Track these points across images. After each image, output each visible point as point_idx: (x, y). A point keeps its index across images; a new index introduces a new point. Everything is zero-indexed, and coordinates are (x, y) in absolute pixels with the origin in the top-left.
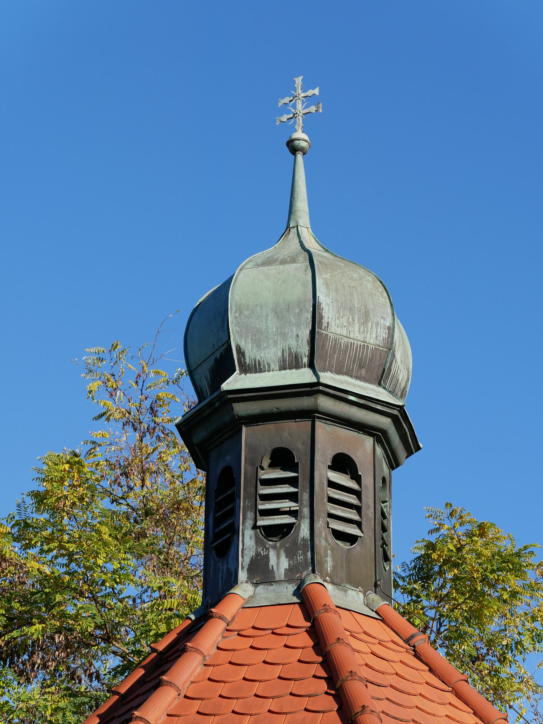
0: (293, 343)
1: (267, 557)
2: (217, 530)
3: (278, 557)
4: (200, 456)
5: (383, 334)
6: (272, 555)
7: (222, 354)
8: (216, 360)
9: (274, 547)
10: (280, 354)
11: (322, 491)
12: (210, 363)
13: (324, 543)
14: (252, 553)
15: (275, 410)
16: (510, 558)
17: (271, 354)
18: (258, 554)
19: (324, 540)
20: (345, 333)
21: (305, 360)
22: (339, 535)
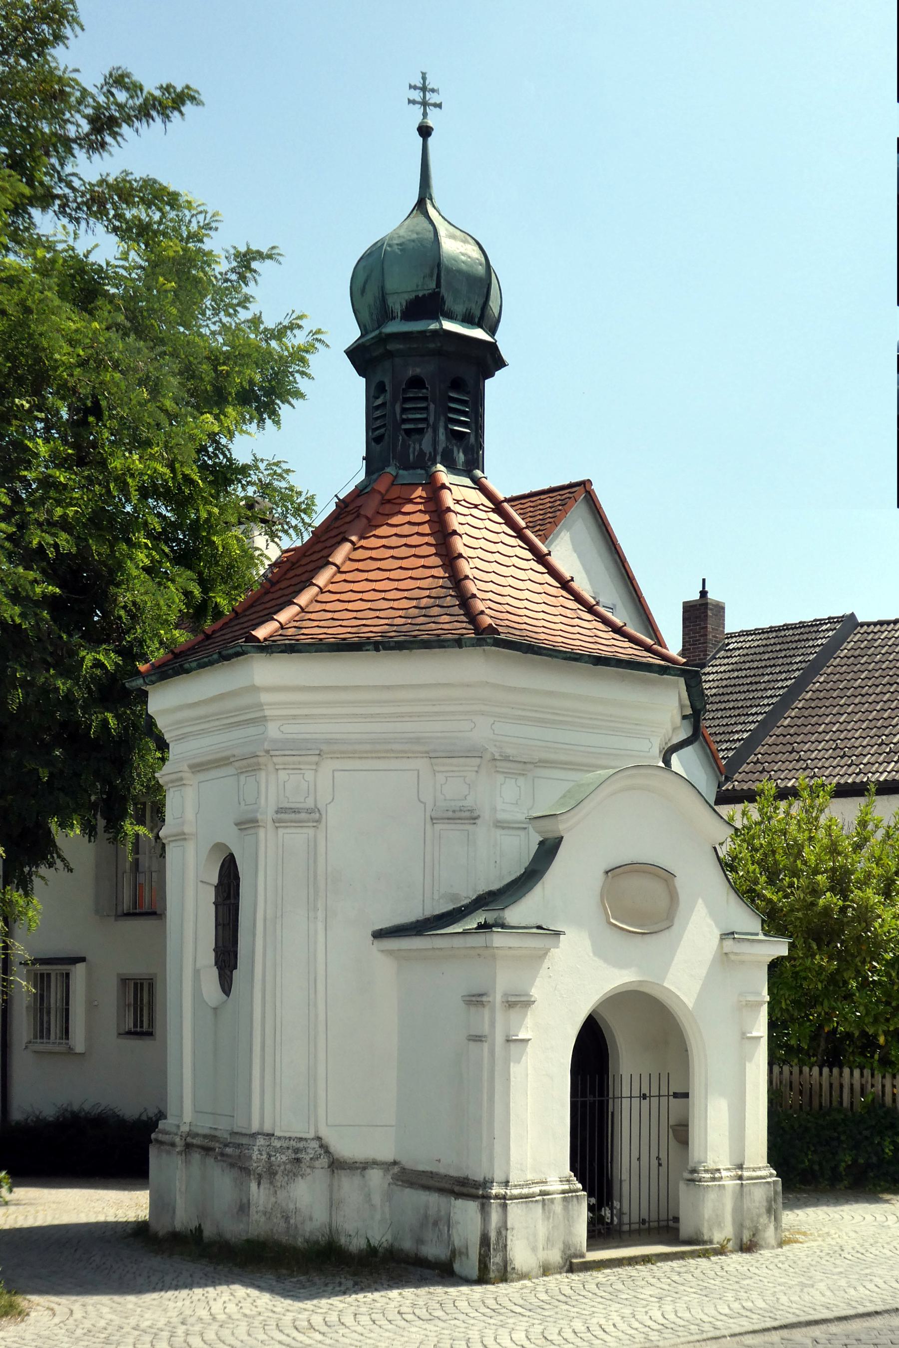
0: (474, 306)
6: (455, 449)
7: (424, 295)
8: (417, 297)
14: (444, 445)
17: (459, 309)
18: (447, 447)
21: (477, 320)
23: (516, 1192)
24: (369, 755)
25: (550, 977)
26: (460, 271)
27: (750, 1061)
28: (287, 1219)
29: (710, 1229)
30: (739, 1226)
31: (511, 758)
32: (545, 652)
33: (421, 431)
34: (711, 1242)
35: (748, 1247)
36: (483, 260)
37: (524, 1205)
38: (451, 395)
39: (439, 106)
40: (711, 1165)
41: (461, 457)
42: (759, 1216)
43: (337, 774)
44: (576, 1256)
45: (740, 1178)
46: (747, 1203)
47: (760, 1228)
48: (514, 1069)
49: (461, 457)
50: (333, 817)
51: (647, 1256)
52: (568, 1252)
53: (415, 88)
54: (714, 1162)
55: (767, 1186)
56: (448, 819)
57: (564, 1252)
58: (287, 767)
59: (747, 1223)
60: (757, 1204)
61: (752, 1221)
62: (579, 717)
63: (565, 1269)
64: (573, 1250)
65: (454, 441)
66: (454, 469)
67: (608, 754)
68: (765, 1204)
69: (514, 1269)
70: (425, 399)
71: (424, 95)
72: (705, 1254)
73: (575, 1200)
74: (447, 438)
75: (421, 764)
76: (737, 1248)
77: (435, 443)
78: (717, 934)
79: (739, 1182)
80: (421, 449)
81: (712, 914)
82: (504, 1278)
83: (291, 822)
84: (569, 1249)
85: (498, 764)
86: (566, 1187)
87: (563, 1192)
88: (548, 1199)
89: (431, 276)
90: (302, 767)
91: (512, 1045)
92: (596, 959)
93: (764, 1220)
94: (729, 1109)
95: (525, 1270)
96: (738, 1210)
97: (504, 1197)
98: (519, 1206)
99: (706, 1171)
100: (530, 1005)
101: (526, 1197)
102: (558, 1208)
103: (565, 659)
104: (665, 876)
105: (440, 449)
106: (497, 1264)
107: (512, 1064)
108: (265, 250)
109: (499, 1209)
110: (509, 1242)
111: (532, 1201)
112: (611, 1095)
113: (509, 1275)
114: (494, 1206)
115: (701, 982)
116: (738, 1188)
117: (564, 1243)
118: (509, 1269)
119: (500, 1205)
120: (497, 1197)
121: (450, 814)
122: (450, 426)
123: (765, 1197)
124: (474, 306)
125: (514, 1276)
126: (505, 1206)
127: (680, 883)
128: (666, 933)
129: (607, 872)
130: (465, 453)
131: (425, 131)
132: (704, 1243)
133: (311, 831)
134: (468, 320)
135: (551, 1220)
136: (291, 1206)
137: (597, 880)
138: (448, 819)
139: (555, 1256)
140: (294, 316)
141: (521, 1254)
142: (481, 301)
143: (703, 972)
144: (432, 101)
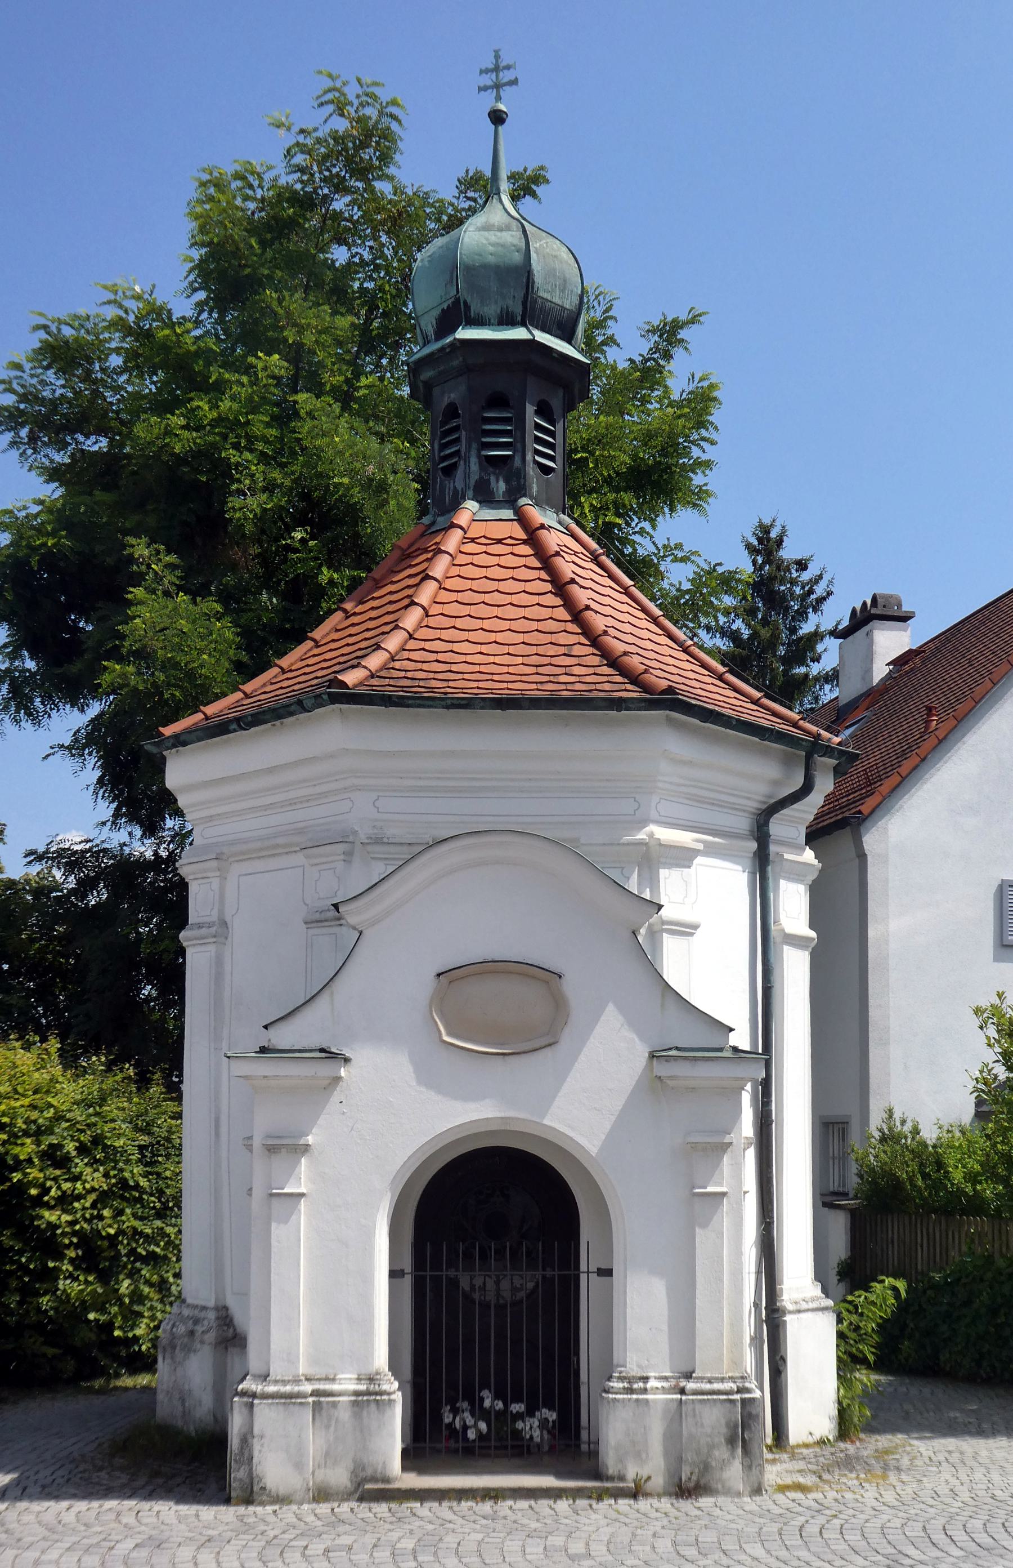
0: (510, 302)
1: (489, 480)
2: (442, 454)
3: (497, 481)
4: (452, 450)
5: (576, 300)
6: (493, 479)
7: (449, 306)
8: (443, 310)
9: (494, 473)
10: (499, 311)
11: (531, 432)
12: (436, 313)
13: (531, 473)
14: (477, 477)
15: (477, 257)
16: (392, 1527)
17: (491, 310)
18: (481, 478)
19: (531, 471)
20: (549, 298)
21: (519, 318)
22: (541, 466)
23: (272, 1389)
24: (264, 853)
25: (344, 1113)
26: (485, 266)
27: (704, 1226)
28: (183, 1400)
29: (621, 1460)
30: (675, 1457)
31: (385, 840)
32: (410, 702)
33: (454, 467)
34: (622, 1478)
35: (685, 1489)
36: (523, 245)
37: (281, 1408)
38: (486, 415)
39: (514, 82)
40: (632, 1369)
41: (501, 487)
42: (712, 1447)
43: (241, 878)
44: (374, 1479)
45: (682, 1391)
46: (688, 1427)
47: (714, 1464)
48: (277, 1231)
49: (501, 487)
50: (239, 928)
51: (494, 1489)
52: (363, 1474)
53: (487, 71)
54: (639, 1366)
55: (728, 1405)
56: (317, 922)
57: (354, 1473)
58: (197, 876)
59: (689, 1456)
60: (709, 1430)
61: (698, 1453)
62: (513, 780)
63: (357, 1496)
64: (369, 1472)
65: (491, 469)
66: (491, 502)
67: (563, 823)
68: (724, 1430)
69: (264, 1489)
70: (457, 429)
71: (498, 77)
72: (618, 1494)
73: (373, 1406)
74: (482, 468)
75: (299, 859)
76: (673, 1489)
77: (467, 476)
78: (642, 1052)
79: (679, 1396)
80: (455, 487)
81: (633, 1023)
82: (248, 1500)
83: (196, 939)
84: (363, 1469)
85: (369, 848)
86: (362, 1387)
87: (357, 1393)
88: (328, 1403)
89: (452, 282)
90: (209, 874)
91: (275, 1201)
92: (423, 1089)
93: (722, 1452)
94: (668, 1294)
95: (282, 1491)
96: (673, 1439)
97: (254, 1395)
98: (273, 1408)
99: (621, 1379)
100: (725, 1151)
101: (290, 1396)
102: (344, 1414)
103: (448, 707)
104: (546, 977)
105: (472, 482)
106: (241, 1480)
107: (274, 1225)
108: (683, 317)
109: (245, 1411)
110: (256, 1454)
111: (294, 1403)
112: (583, 1267)
113: (255, 1497)
114: (236, 1406)
115: (613, 1118)
116: (675, 1405)
117: (354, 1461)
118: (256, 1488)
119: (246, 1404)
120: (244, 1394)
121: (317, 916)
122: (484, 453)
123: (723, 1421)
124: (510, 302)
125: (264, 1498)
126: (251, 1406)
127: (570, 987)
128: (547, 1052)
129: (439, 975)
130: (507, 481)
131: (497, 118)
132: (610, 1478)
133: (212, 948)
134: (507, 320)
135: (332, 1429)
136: (186, 1387)
137: (424, 984)
138: (317, 922)
139: (339, 1477)
140: (696, 380)
141: (272, 1467)
142: (520, 294)
143: (617, 1103)
144: (505, 80)
